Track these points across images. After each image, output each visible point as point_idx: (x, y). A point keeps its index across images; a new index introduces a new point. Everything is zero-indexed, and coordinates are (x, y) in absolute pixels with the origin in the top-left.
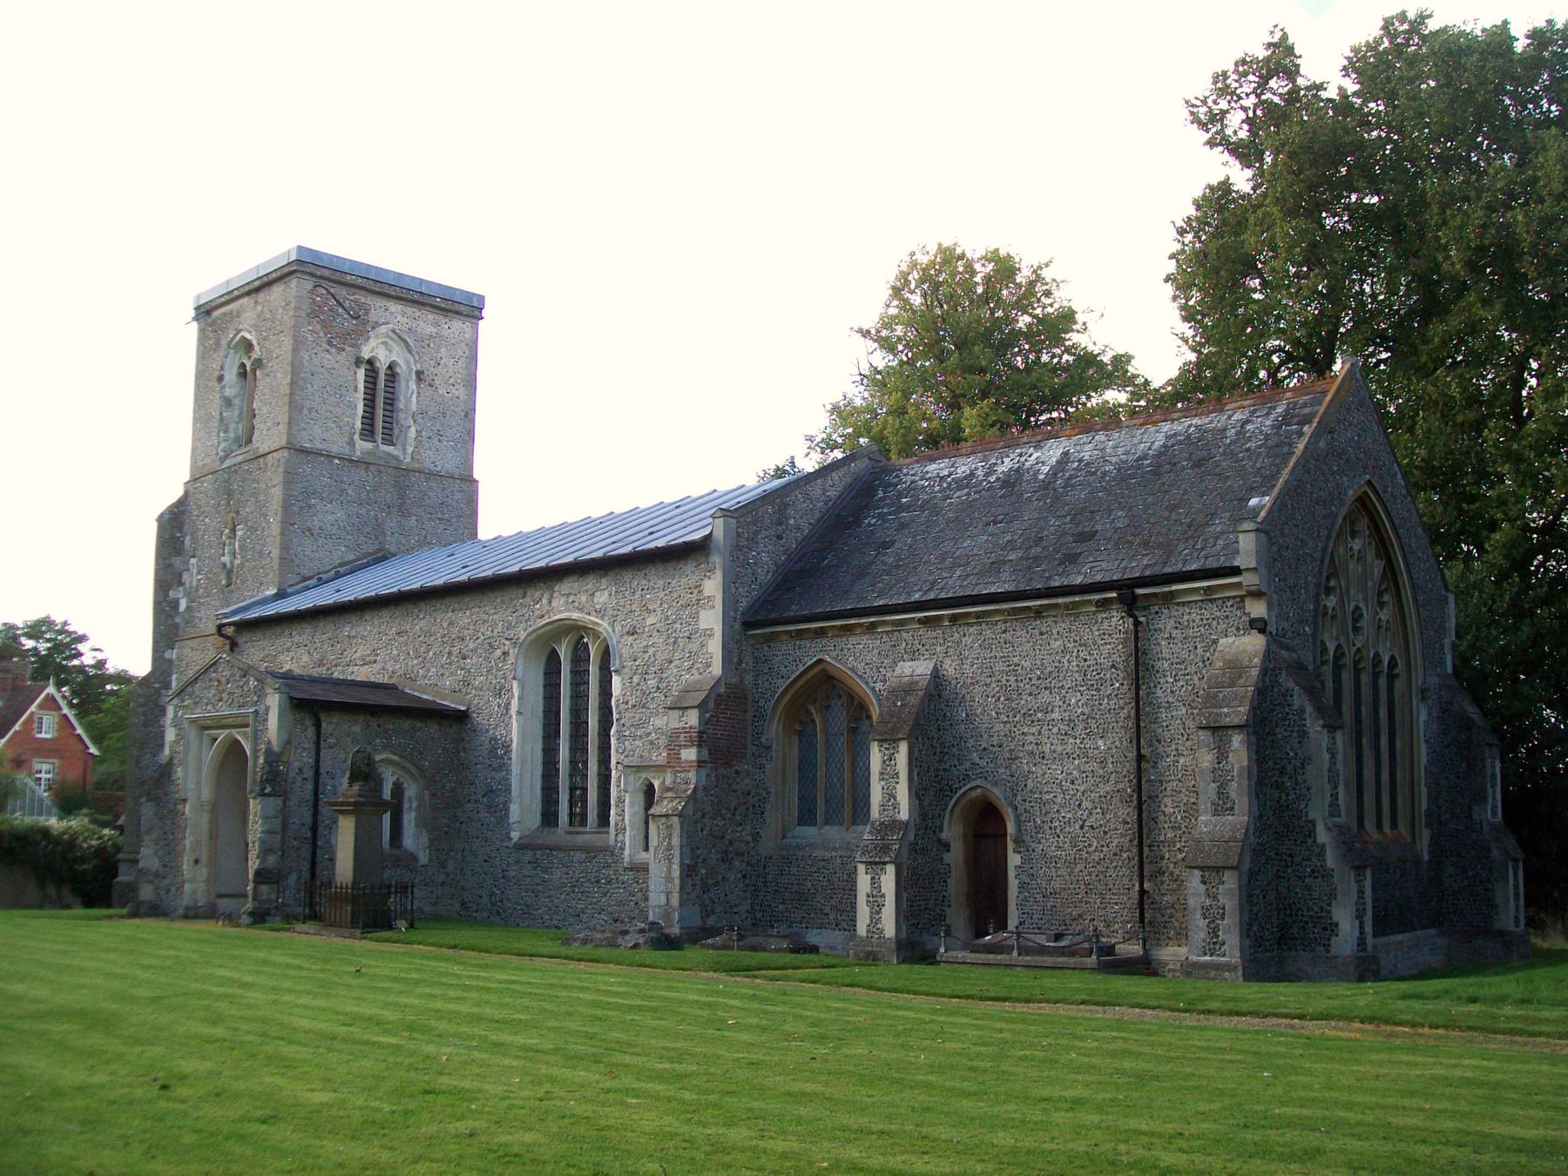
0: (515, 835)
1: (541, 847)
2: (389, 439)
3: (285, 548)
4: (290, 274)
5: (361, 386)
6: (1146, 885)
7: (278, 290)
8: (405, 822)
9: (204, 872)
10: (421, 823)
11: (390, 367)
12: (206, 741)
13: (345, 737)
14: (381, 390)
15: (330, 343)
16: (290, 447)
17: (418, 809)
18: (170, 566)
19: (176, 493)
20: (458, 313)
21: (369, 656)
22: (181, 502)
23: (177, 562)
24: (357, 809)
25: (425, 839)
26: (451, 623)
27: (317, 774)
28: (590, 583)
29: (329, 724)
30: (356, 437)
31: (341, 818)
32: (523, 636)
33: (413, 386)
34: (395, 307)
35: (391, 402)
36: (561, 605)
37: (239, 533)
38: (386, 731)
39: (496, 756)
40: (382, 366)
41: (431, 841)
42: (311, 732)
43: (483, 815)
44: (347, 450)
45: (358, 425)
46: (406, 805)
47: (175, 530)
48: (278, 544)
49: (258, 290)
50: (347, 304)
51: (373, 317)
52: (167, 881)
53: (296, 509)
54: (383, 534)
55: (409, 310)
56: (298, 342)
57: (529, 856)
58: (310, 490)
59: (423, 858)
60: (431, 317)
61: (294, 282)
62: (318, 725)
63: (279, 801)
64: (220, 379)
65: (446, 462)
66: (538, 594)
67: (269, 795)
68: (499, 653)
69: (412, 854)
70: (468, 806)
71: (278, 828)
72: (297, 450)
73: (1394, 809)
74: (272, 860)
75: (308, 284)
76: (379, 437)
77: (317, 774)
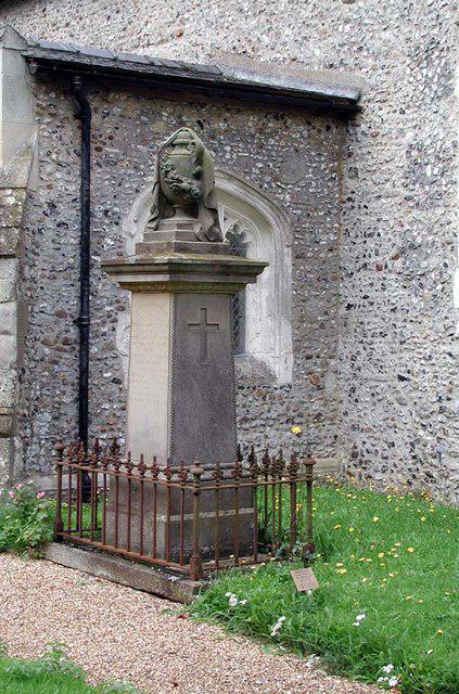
29: (113, 117)
42: (70, 132)
43: (396, 293)
59: (283, 370)
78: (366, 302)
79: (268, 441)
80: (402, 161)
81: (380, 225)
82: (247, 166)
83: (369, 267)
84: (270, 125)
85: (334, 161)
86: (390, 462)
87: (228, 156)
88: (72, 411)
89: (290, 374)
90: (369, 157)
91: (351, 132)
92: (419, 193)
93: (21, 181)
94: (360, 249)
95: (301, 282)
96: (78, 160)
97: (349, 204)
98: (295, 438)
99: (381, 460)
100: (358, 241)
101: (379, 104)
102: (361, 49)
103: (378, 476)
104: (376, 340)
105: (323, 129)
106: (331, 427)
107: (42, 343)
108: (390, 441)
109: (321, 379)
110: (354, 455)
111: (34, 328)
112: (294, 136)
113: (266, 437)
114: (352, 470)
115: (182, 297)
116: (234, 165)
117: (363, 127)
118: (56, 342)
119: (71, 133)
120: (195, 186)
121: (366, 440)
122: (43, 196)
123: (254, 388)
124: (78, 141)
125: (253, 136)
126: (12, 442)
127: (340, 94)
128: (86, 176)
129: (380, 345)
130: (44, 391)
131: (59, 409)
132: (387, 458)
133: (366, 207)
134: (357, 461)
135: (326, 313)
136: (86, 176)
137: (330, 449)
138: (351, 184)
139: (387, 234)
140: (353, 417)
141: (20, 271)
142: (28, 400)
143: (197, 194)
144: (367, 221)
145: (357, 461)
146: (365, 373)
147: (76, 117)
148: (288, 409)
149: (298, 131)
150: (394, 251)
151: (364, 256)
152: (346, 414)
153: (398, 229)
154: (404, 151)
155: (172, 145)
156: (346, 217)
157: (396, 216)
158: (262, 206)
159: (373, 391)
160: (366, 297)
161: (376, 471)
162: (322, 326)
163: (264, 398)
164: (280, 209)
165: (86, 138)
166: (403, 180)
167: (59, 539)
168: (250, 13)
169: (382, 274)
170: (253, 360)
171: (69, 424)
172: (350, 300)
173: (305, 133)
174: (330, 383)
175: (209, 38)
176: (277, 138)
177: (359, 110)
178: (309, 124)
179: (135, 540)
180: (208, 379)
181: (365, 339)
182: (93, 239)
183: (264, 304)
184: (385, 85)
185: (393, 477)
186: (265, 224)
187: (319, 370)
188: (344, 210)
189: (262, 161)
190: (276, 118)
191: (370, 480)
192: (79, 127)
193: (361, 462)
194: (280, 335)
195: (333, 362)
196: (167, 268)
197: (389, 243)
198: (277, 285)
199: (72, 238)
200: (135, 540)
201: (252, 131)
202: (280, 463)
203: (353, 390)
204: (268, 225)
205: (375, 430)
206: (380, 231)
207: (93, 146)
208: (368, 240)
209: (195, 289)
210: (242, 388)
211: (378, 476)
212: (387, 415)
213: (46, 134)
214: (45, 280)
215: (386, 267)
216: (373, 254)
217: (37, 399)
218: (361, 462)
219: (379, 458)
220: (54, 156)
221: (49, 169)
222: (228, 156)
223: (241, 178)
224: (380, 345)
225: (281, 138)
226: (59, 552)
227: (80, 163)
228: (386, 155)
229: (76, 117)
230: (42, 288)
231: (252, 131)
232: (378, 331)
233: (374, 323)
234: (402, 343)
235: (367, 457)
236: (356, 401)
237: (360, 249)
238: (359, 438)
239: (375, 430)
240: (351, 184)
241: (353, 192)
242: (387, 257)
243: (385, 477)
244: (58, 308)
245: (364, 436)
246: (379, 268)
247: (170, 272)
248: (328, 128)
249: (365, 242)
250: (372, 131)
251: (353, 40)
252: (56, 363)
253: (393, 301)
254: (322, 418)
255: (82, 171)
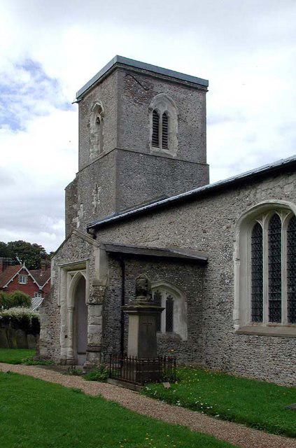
0: (236, 326)
1: (253, 334)
2: (165, 146)
3: (118, 193)
4: (115, 69)
5: (151, 122)
7: (110, 79)
9: (69, 342)
11: (165, 114)
13: (142, 274)
14: (160, 124)
15: (135, 101)
16: (121, 151)
18: (72, 208)
19: (72, 177)
20: (196, 89)
21: (155, 235)
22: (75, 181)
23: (75, 206)
24: (140, 312)
25: (185, 327)
26: (197, 215)
27: (123, 293)
28: (281, 182)
29: (130, 267)
30: (150, 145)
32: (238, 216)
33: (176, 123)
34: (166, 85)
35: (165, 130)
36: (263, 196)
37: (99, 191)
38: (162, 270)
39: (224, 284)
40: (161, 113)
42: (119, 270)
43: (218, 315)
44: (146, 151)
45: (151, 139)
47: (72, 191)
49: (101, 82)
50: (142, 83)
51: (155, 89)
52: (53, 346)
54: (165, 189)
55: (173, 87)
56: (120, 102)
57: (244, 338)
59: (184, 337)
60: (183, 90)
61: (116, 73)
64: (89, 126)
65: (194, 157)
66: (247, 193)
68: (224, 227)
72: (121, 151)
73: (275, 267)
75: (124, 74)
76: (161, 145)
77: (123, 293)
80: (219, 278)
82: (172, 279)
88: (119, 346)
92: (224, 287)
93: (104, 284)
95: (190, 312)
122: (111, 288)
127: (202, 258)
128: (123, 283)
136: (123, 283)
138: (205, 284)
141: (103, 308)
149: (189, 270)
155: (140, 278)
158: (177, 290)
164: (183, 291)
165: (123, 273)
167: (110, 377)
171: (118, 350)
174: (199, 341)
175: (167, 240)
177: (208, 263)
179: (129, 377)
180: (147, 337)
182: (126, 300)
186: (178, 295)
197: (216, 300)
199: (119, 299)
200: (129, 377)
202: (162, 358)
204: (179, 295)
209: (145, 314)
224: (213, 330)
226: (110, 381)
233: (212, 323)
238: (208, 357)
240: (205, 284)
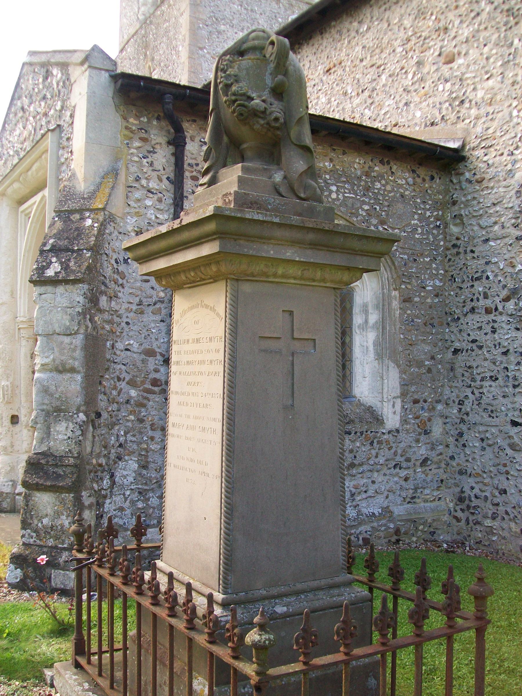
6: (291, 358)
8: (357, 352)
10: (384, 351)
12: (21, 218)
17: (382, 326)
25: (393, 379)
31: (181, 303)
41: (405, 385)
42: (163, 157)
46: (358, 320)
48: (186, 69)
53: (204, 33)
58: (219, 15)
59: (392, 419)
62: (178, 143)
63: (76, 295)
67: (54, 282)
69: (370, 410)
70: (473, 320)
71: (77, 359)
74: (63, 433)
78: (474, 346)
79: (376, 486)
81: (488, 268)
83: (477, 311)
84: (376, 168)
85: (438, 210)
86: (501, 508)
87: (334, 196)
89: (398, 418)
90: (475, 202)
91: (455, 181)
94: (466, 293)
96: (171, 187)
97: (455, 251)
98: (403, 483)
99: (491, 507)
100: (464, 286)
101: (483, 150)
102: (462, 102)
103: (488, 522)
104: (486, 384)
105: (427, 178)
106: (437, 470)
107: (128, 383)
108: (500, 487)
109: (428, 423)
110: (461, 500)
111: (119, 367)
112: (400, 182)
113: (373, 482)
114: (459, 514)
115: (246, 288)
116: (340, 205)
117: (467, 175)
118: (143, 383)
119: (164, 160)
120: (276, 109)
121: (474, 485)
123: (362, 433)
124: (172, 168)
125: (359, 178)
126: (78, 500)
129: (490, 390)
130: (129, 437)
131: (146, 456)
132: (497, 505)
133: (472, 251)
134: (464, 506)
135: (433, 358)
137: (435, 493)
139: (496, 276)
140: (460, 460)
142: (105, 447)
143: (276, 119)
144: (475, 265)
145: (464, 506)
146: (473, 418)
147: (169, 143)
148: (395, 454)
150: (504, 293)
151: (472, 300)
152: (452, 458)
153: (510, 270)
154: (513, 192)
156: (451, 263)
157: (506, 257)
159: (483, 436)
160: (474, 341)
161: (485, 517)
162: (429, 371)
163: (372, 444)
166: (513, 221)
168: (353, 94)
169: (491, 317)
170: (360, 404)
172: (457, 345)
173: (410, 180)
176: (383, 182)
178: (414, 171)
181: (473, 384)
183: (371, 348)
184: (490, 131)
185: (505, 526)
187: (426, 414)
188: (449, 257)
189: (368, 204)
190: (382, 162)
191: (478, 527)
192: (173, 154)
193: (468, 507)
194: (387, 379)
195: (439, 407)
196: (211, 227)
198: (384, 328)
201: (359, 173)
203: (461, 434)
205: (485, 476)
206: (489, 274)
207: (187, 174)
208: (476, 284)
210: (350, 433)
211: (488, 522)
212: (498, 461)
213: (136, 159)
214: (132, 315)
215: (496, 309)
216: (481, 298)
217: (121, 445)
218: (468, 507)
219: (489, 505)
220: (144, 182)
221: (137, 195)
222: (334, 196)
223: (347, 218)
224: (490, 390)
225: (387, 183)
227: (172, 191)
228: (492, 198)
229: (169, 143)
230: (128, 323)
231: (359, 173)
232: (488, 375)
234: (515, 387)
235: (475, 502)
236: (464, 445)
237: (466, 293)
238: (468, 482)
239: (485, 476)
241: (458, 239)
242: (497, 300)
243: (496, 524)
244: (146, 346)
245: (471, 481)
246: (488, 311)
247: (217, 235)
248: (432, 178)
249: (472, 286)
250: (477, 177)
251: (454, 95)
252: (144, 406)
253: (506, 344)
254: (429, 462)
255: (175, 199)
